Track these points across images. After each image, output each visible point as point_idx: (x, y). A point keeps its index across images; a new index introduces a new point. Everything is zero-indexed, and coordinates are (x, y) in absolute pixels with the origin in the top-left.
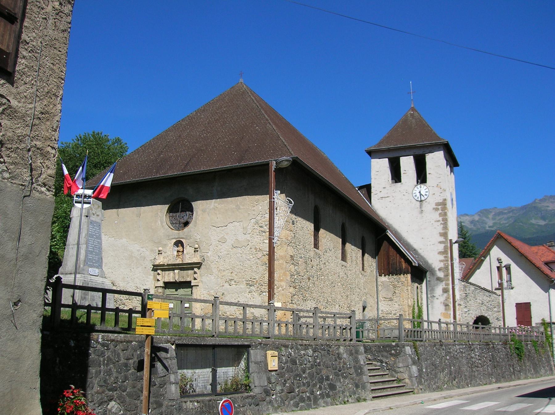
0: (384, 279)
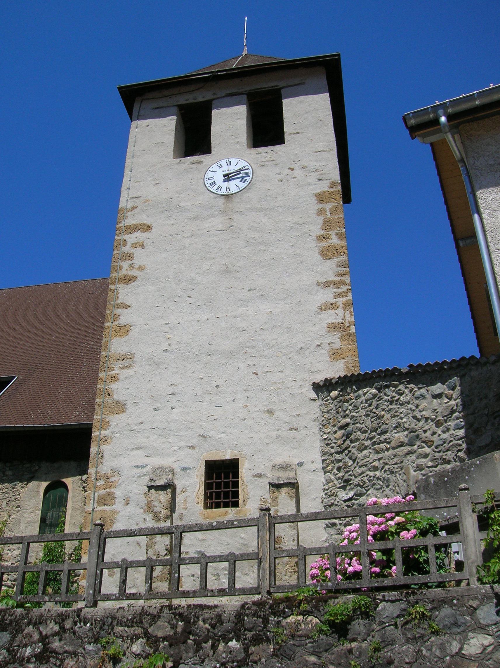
0: (42, 524)
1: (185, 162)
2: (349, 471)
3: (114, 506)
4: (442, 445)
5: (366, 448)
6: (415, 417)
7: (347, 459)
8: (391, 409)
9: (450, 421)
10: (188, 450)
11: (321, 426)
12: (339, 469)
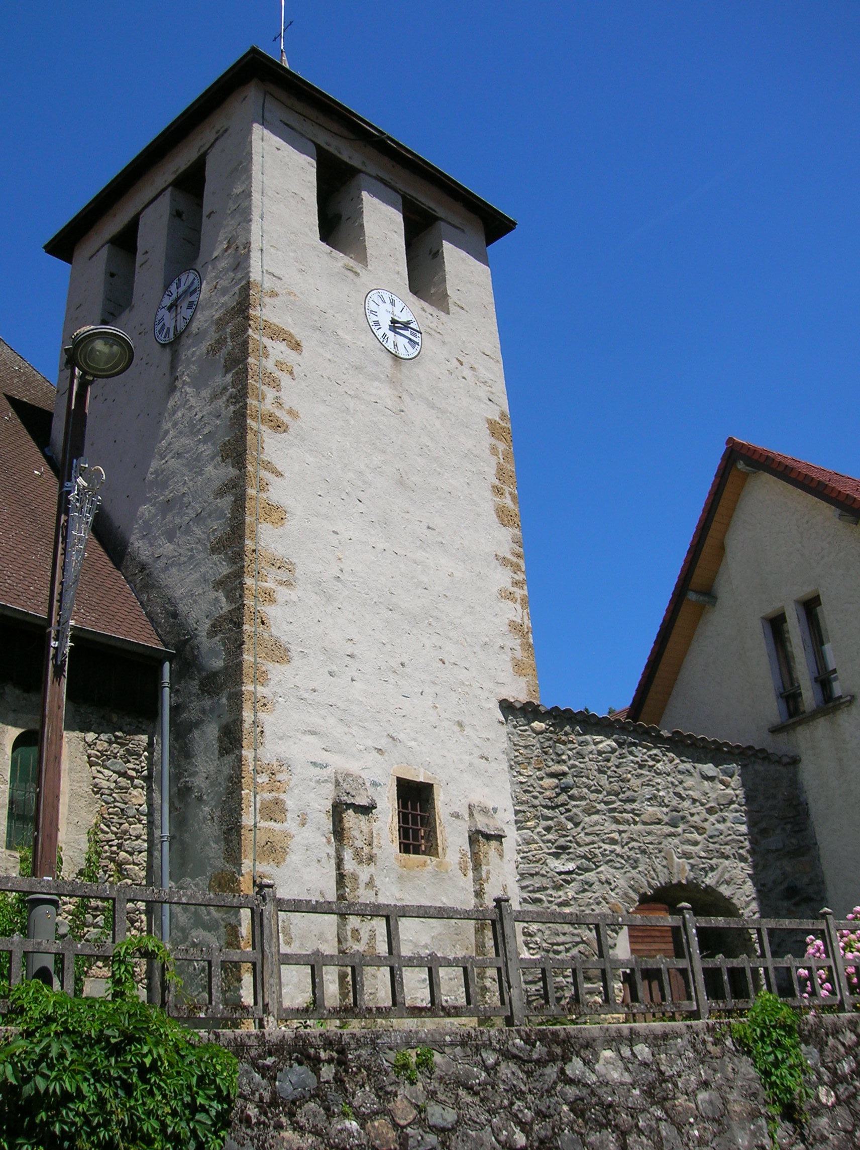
1: (336, 259)
2: (567, 836)
3: (285, 824)
4: (718, 836)
5: (597, 812)
6: (678, 795)
7: (562, 818)
8: (642, 774)
9: (726, 811)
10: (375, 753)
11: (512, 763)
12: (548, 829)
